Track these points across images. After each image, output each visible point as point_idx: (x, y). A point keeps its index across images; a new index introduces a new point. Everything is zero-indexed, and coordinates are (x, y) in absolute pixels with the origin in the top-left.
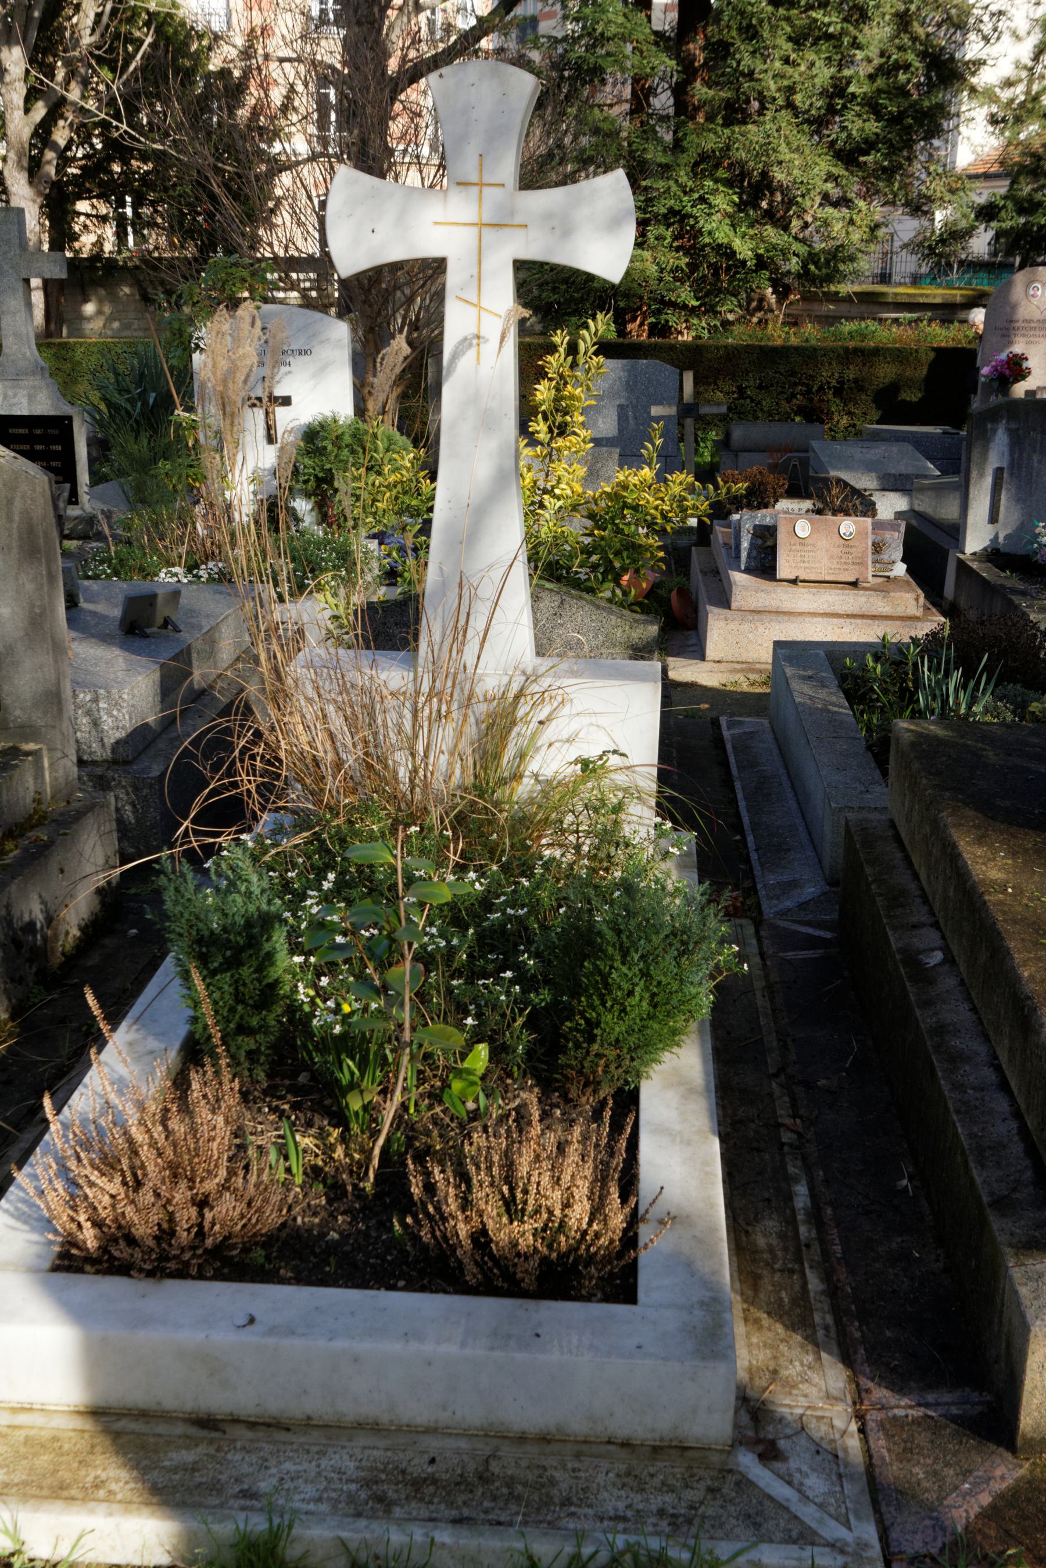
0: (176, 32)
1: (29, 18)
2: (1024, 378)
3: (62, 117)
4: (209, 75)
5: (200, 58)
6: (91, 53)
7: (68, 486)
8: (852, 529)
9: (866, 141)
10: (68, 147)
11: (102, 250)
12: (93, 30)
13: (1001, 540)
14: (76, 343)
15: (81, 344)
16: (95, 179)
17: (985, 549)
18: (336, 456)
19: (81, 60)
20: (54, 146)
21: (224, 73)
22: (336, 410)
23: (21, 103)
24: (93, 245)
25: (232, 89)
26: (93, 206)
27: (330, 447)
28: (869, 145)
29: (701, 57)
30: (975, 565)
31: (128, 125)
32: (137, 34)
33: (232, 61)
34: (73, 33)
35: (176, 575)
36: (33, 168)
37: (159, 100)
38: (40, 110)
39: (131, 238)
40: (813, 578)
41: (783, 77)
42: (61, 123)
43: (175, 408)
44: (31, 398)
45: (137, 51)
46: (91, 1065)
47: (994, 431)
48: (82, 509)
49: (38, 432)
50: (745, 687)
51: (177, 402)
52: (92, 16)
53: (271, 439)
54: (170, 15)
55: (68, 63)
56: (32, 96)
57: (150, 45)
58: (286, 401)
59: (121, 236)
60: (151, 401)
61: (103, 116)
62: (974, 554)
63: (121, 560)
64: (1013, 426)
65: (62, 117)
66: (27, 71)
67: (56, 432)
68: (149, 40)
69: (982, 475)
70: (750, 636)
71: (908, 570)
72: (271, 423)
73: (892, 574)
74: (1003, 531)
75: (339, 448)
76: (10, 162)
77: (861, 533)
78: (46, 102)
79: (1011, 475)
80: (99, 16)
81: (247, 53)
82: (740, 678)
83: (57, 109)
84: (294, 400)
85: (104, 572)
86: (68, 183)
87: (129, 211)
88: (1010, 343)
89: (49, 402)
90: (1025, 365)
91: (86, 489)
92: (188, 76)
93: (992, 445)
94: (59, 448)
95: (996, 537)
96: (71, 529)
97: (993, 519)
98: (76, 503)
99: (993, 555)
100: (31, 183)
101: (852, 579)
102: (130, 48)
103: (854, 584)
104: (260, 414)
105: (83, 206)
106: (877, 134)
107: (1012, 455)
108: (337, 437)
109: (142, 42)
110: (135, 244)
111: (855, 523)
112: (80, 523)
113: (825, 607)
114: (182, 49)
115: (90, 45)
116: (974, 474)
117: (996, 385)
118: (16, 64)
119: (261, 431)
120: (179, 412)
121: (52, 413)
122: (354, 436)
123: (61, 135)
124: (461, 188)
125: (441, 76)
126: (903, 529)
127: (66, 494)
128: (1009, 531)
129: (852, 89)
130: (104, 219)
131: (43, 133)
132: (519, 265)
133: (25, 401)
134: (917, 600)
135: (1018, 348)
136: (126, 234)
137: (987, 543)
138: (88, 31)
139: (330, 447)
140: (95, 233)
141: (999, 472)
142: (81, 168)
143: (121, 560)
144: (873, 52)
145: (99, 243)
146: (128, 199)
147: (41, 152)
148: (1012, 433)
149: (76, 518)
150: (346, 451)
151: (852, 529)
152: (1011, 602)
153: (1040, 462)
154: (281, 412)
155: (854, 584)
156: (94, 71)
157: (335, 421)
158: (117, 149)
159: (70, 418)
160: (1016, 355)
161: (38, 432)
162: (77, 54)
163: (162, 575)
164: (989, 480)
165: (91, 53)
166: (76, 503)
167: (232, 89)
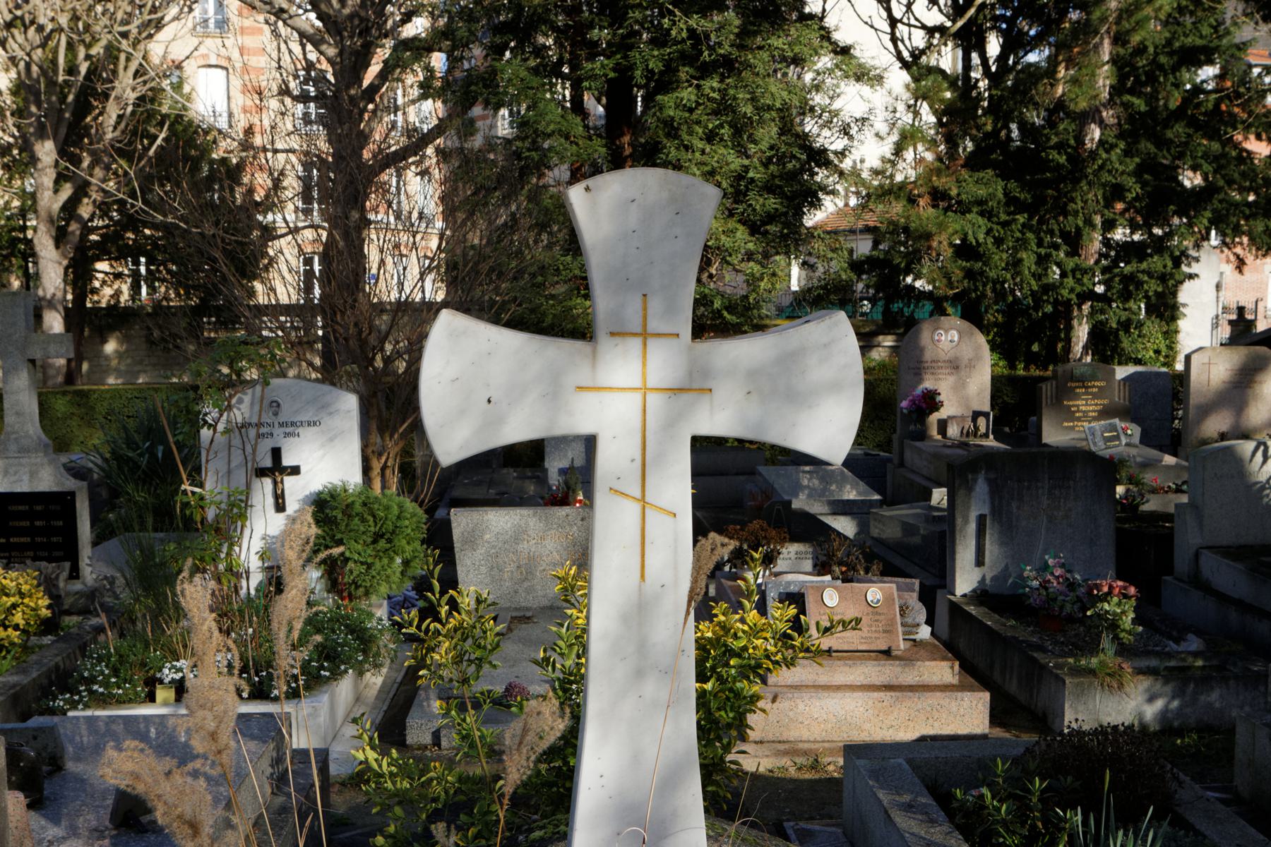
0: (184, 130)
1: (60, 118)
2: (937, 410)
3: (87, 195)
4: (212, 162)
5: (205, 151)
6: (112, 146)
7: (67, 565)
8: (879, 596)
9: (768, 213)
10: (91, 220)
11: (119, 302)
12: (115, 128)
13: (988, 581)
14: (90, 390)
15: (94, 391)
16: (112, 246)
17: (974, 591)
18: (347, 525)
19: (104, 151)
20: (79, 219)
21: (224, 161)
22: (345, 479)
23: (51, 185)
24: (112, 296)
25: (232, 173)
26: (112, 266)
27: (340, 516)
28: (771, 218)
29: (628, 151)
30: (972, 609)
31: (145, 202)
32: (153, 130)
33: (231, 152)
34: (97, 130)
35: (180, 670)
36: (60, 238)
37: (169, 181)
38: (67, 191)
39: (144, 290)
40: (846, 648)
41: (705, 164)
42: (86, 200)
43: (182, 482)
44: (33, 475)
45: (151, 144)
46: (111, 820)
47: (975, 481)
48: (84, 583)
49: (39, 508)
50: (793, 772)
51: (184, 477)
52: (114, 117)
53: (280, 507)
54: (181, 116)
55: (93, 153)
56: (60, 179)
57: (164, 140)
58: (295, 471)
59: (135, 288)
60: (160, 455)
61: (121, 196)
62: (964, 595)
63: (121, 656)
64: (992, 476)
65: (87, 195)
66: (57, 161)
67: (58, 508)
68: (163, 135)
69: (966, 522)
70: (791, 714)
71: (932, 634)
72: (279, 492)
73: (918, 637)
74: (989, 571)
75: (349, 516)
76: (39, 233)
77: (888, 599)
78: (73, 184)
79: (993, 520)
80: (120, 117)
81: (246, 145)
82: (785, 761)
83: (82, 190)
84: (303, 469)
85: (102, 673)
86: (90, 248)
87: (143, 269)
88: (921, 381)
89: (52, 478)
90: (938, 399)
91: (88, 561)
92: (196, 168)
93: (973, 494)
94: (61, 523)
95: (984, 578)
96: (72, 605)
97: (979, 562)
98: (77, 577)
99: (981, 596)
100: (57, 247)
101: (884, 648)
102: (146, 142)
103: (887, 653)
104: (268, 483)
105: (103, 266)
106: (776, 209)
107: (992, 503)
108: (347, 506)
109: (156, 137)
110: (148, 294)
111: (881, 589)
112: (82, 596)
113: (862, 678)
114: (190, 142)
115: (112, 139)
116: (959, 521)
117: (914, 416)
118: (47, 154)
119: (270, 500)
120: (186, 486)
121: (55, 489)
122: (365, 504)
123: (85, 210)
124: (618, 340)
125: (587, 189)
126: (917, 587)
127: (65, 574)
128: (995, 573)
129: (751, 174)
130: (118, 276)
131: (70, 208)
132: (701, 445)
133: (26, 478)
134: (952, 668)
135: (928, 384)
136: (140, 287)
137: (975, 585)
138: (111, 129)
139: (340, 516)
140: (111, 285)
141: (981, 520)
142: (101, 236)
143: (121, 656)
144: (764, 145)
145: (118, 293)
146: (143, 260)
147: (68, 225)
148: (990, 482)
149: (77, 593)
150: (356, 520)
151: (879, 596)
152: (1035, 660)
153: (1018, 508)
154: (289, 481)
155: (887, 653)
156: (115, 160)
157: (346, 491)
158: (131, 222)
159: (72, 494)
160: (930, 391)
161: (39, 508)
162: (101, 146)
163: (166, 671)
164: (972, 527)
165: (112, 146)
166: (77, 577)
167: (232, 173)
